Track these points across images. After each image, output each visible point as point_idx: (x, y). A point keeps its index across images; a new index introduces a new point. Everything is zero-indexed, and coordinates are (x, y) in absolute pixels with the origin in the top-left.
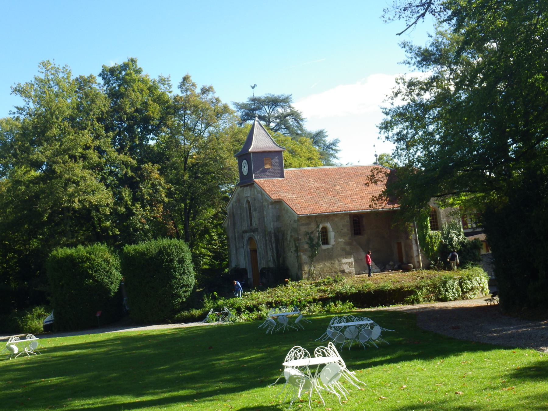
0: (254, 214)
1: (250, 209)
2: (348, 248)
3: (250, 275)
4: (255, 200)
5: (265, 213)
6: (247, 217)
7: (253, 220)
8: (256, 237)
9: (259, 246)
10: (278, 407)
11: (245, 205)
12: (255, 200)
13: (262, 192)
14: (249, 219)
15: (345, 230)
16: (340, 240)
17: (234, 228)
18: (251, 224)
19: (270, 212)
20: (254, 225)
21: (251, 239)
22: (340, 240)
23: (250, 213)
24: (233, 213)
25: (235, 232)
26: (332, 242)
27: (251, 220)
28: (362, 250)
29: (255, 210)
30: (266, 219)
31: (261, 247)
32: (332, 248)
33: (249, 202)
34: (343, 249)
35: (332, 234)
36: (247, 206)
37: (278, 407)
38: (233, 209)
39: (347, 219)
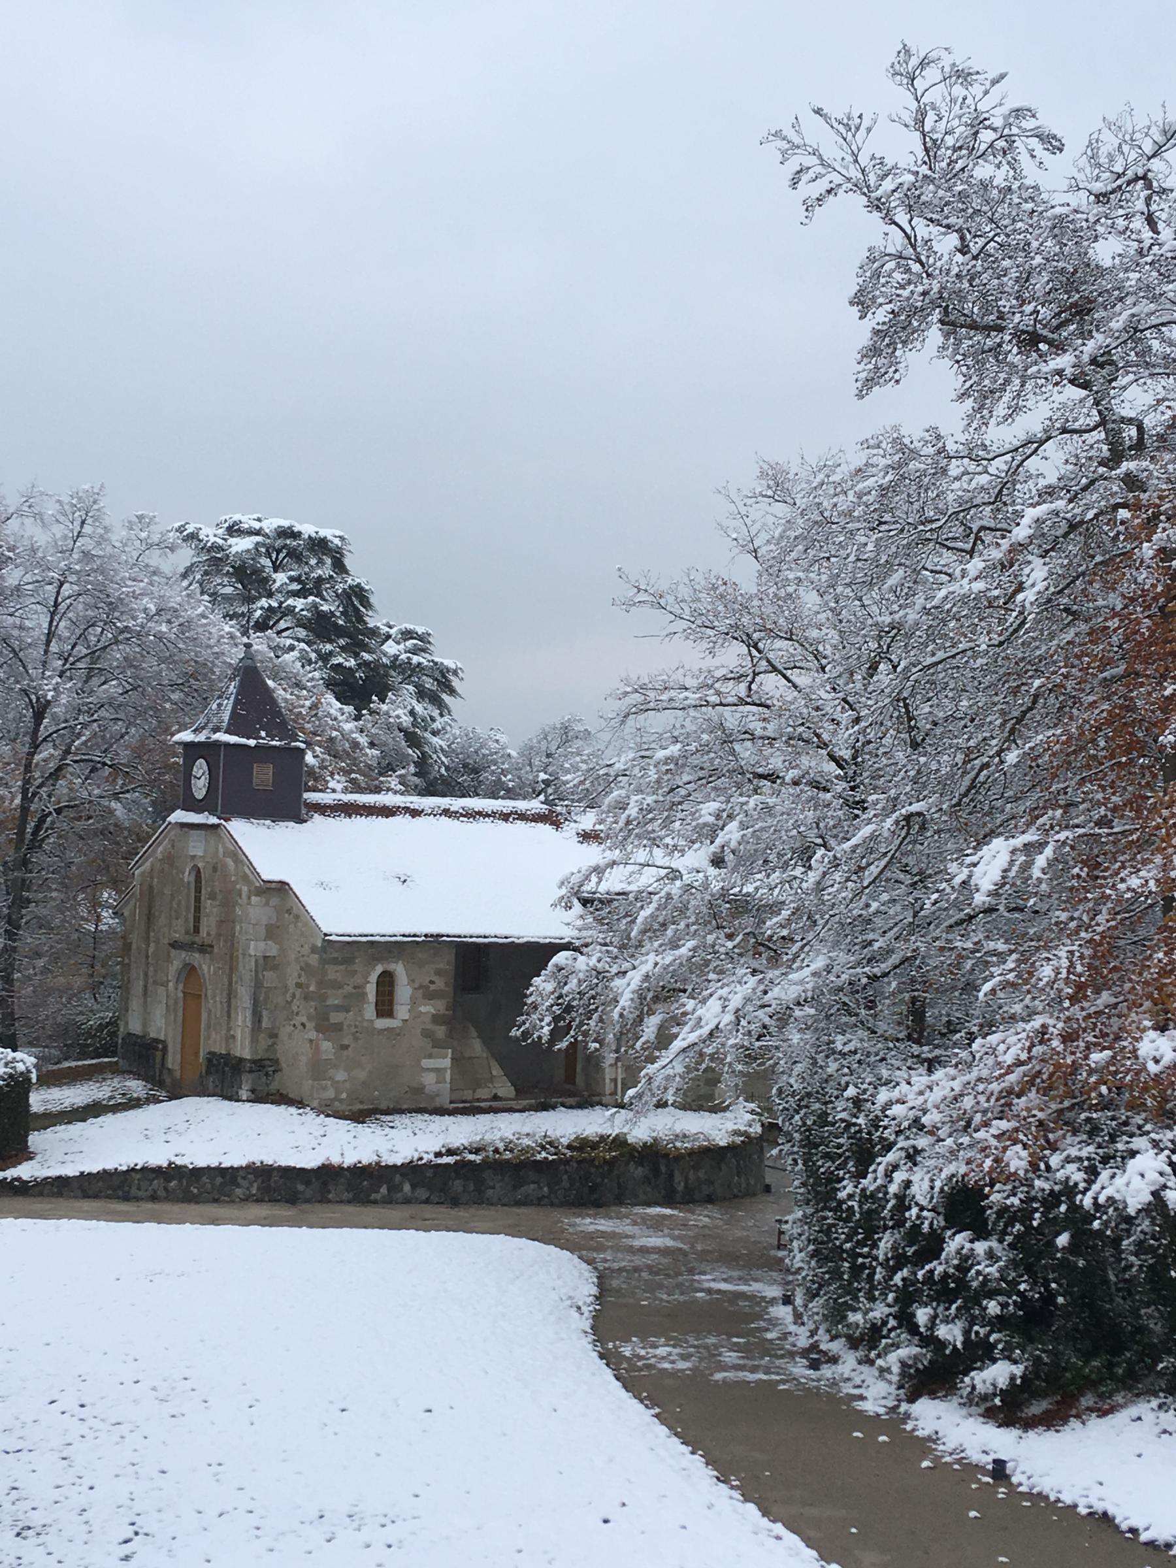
0: (207, 904)
1: (198, 890)
2: (441, 1031)
3: (173, 1061)
4: (215, 869)
5: (238, 911)
6: (188, 909)
7: (204, 922)
8: (205, 967)
9: (209, 992)
10: (917, 1433)
11: (188, 877)
12: (215, 869)
13: (237, 854)
14: (191, 917)
15: (440, 984)
16: (423, 1009)
17: (148, 931)
18: (197, 930)
19: (256, 912)
20: (203, 933)
21: (190, 971)
22: (423, 1009)
23: (198, 899)
24: (151, 887)
25: (148, 938)
26: (402, 1011)
27: (197, 920)
28: (475, 1034)
29: (212, 896)
30: (238, 928)
31: (214, 997)
32: (401, 1028)
33: (199, 871)
34: (426, 1034)
35: (403, 992)
36: (192, 879)
37: (917, 1433)
38: (152, 878)
39: (446, 962)
